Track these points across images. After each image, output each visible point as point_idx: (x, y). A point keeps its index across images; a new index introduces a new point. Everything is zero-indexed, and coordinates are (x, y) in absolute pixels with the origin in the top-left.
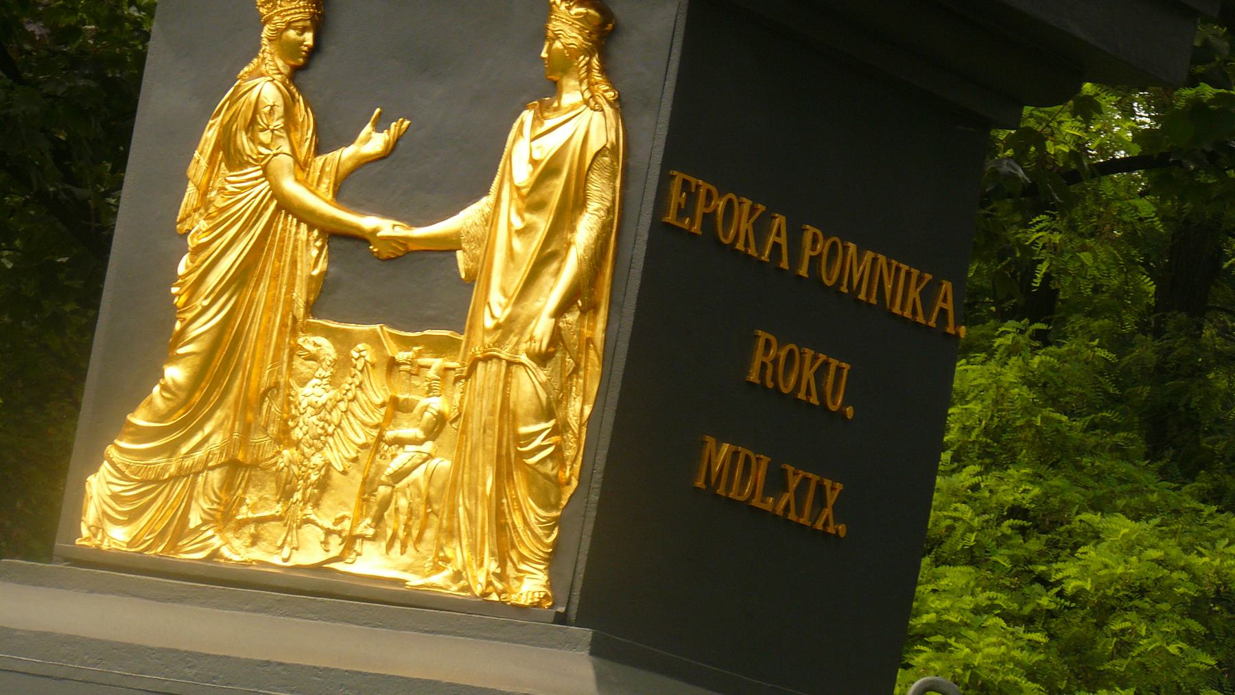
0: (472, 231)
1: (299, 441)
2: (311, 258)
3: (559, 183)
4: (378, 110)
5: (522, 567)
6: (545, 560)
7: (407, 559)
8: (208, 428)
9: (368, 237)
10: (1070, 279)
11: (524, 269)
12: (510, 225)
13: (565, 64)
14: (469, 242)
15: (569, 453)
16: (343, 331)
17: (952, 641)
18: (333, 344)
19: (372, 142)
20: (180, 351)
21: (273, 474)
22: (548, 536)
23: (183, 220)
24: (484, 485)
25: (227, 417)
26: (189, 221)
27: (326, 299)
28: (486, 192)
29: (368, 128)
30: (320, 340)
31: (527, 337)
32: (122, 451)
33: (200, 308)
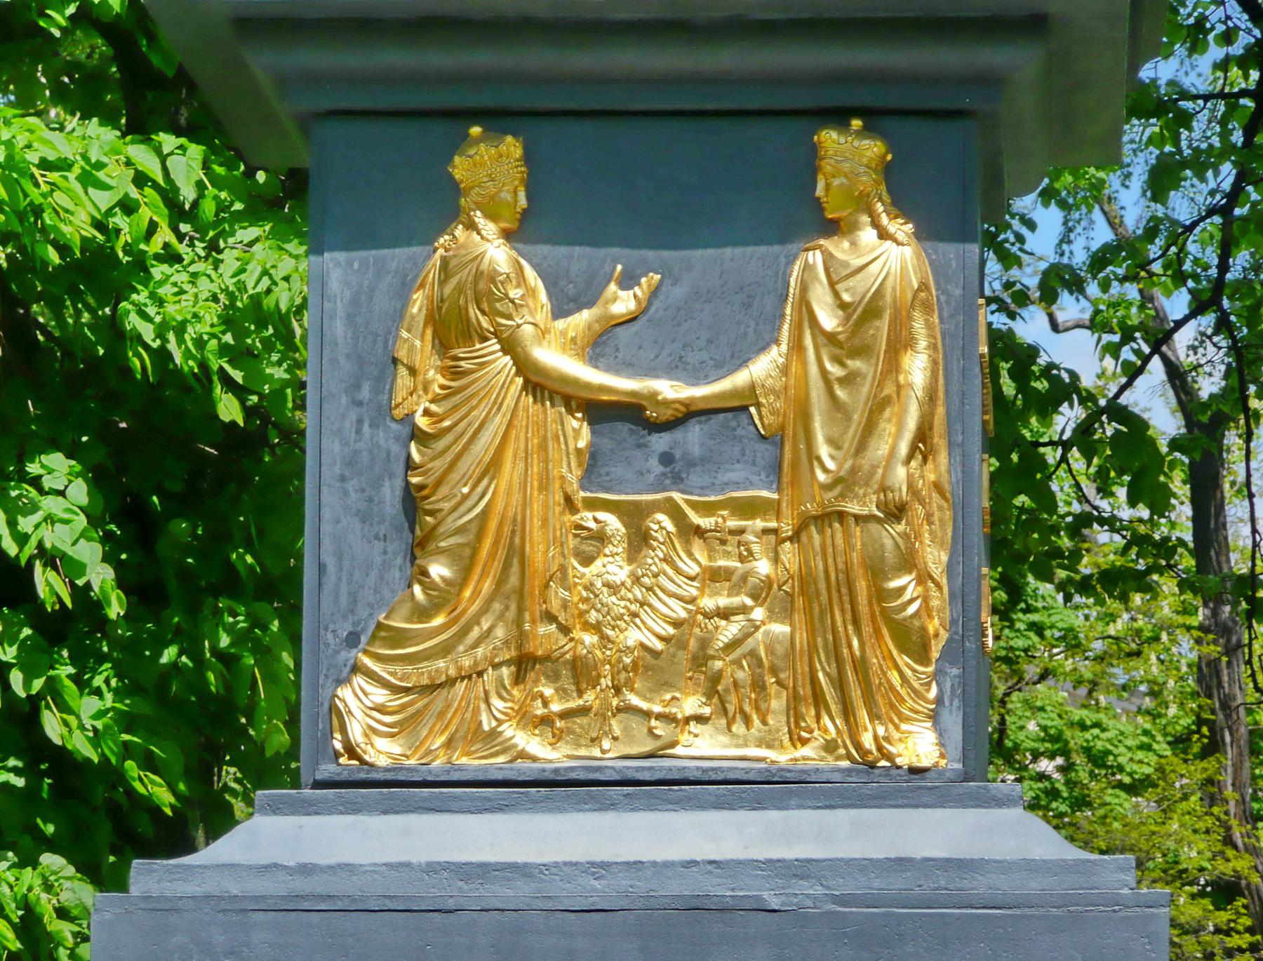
0: (770, 382)
3: (884, 324)
5: (904, 727)
6: (930, 717)
9: (644, 403)
12: (824, 373)
15: (935, 603)
17: (51, 673)
23: (397, 406)
24: (850, 646)
29: (613, 287)
30: (602, 515)
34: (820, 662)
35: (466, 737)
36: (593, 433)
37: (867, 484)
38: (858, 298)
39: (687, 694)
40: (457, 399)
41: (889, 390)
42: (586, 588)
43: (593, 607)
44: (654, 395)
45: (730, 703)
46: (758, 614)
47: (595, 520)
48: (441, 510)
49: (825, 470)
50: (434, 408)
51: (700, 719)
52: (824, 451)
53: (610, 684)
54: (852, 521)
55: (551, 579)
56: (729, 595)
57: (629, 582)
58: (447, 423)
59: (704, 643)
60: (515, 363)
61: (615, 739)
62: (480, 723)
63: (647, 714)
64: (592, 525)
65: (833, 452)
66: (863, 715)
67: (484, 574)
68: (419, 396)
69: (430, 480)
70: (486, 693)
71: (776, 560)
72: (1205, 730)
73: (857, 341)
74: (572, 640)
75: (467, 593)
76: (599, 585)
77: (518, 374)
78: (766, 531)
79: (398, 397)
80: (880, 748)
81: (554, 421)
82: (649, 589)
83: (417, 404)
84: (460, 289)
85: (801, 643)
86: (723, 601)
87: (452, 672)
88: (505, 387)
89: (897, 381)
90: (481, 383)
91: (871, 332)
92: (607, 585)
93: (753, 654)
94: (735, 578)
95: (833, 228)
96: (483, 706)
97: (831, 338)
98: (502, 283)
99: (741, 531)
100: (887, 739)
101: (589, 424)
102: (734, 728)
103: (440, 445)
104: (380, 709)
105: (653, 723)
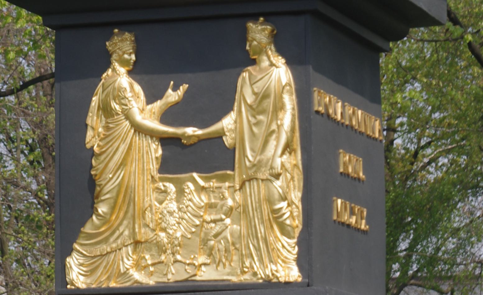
1: (166, 228)
2: (156, 151)
4: (172, 83)
7: (227, 270)
8: (121, 229)
9: (181, 137)
10: (163, 223)
11: (261, 139)
13: (261, 51)
14: (229, 131)
15: (295, 214)
16: (178, 178)
18: (173, 184)
19: (173, 96)
20: (103, 198)
21: (155, 244)
22: (294, 250)
23: (88, 143)
25: (129, 223)
26: (91, 142)
27: (167, 166)
28: (231, 109)
29: (170, 91)
30: (167, 184)
31: (269, 167)
32: (82, 245)
33: (108, 178)
34: (251, 240)
35: (115, 276)
36: (163, 150)
37: (266, 167)
38: (260, 91)
39: (200, 255)
40: (108, 140)
41: (274, 127)
42: (161, 214)
43: (163, 221)
44: (184, 134)
45: (217, 258)
46: (228, 221)
47: (164, 186)
48: (101, 184)
49: (250, 161)
50: (101, 143)
51: (205, 264)
52: (249, 153)
53: (170, 252)
54: (260, 181)
55: (146, 210)
56: (216, 214)
57: (177, 211)
58: (104, 149)
59: (206, 234)
60: (130, 123)
61: (173, 274)
62: (120, 270)
63: (185, 263)
64: (163, 188)
65: (253, 154)
66: (266, 260)
67: (120, 209)
68: (96, 139)
69: (98, 172)
70: (122, 258)
71: (234, 199)
72: (20, 240)
73: (260, 108)
74: (156, 234)
75: (114, 217)
76: (165, 212)
77: (132, 126)
78: (229, 187)
79: (87, 140)
80: (273, 274)
81: (146, 146)
82: (185, 213)
83: (96, 142)
84: (108, 95)
85: (244, 233)
86: (213, 217)
87: (109, 250)
88: (127, 134)
89: (277, 124)
90: (117, 133)
91: (266, 104)
92: (168, 212)
93: (225, 238)
94: (219, 207)
95: (253, 62)
96: (121, 263)
97: (251, 106)
98: (123, 92)
99: (220, 188)
100: (277, 271)
101: (162, 146)
102: (219, 268)
103: (103, 157)
104: (81, 265)
105: (187, 267)
